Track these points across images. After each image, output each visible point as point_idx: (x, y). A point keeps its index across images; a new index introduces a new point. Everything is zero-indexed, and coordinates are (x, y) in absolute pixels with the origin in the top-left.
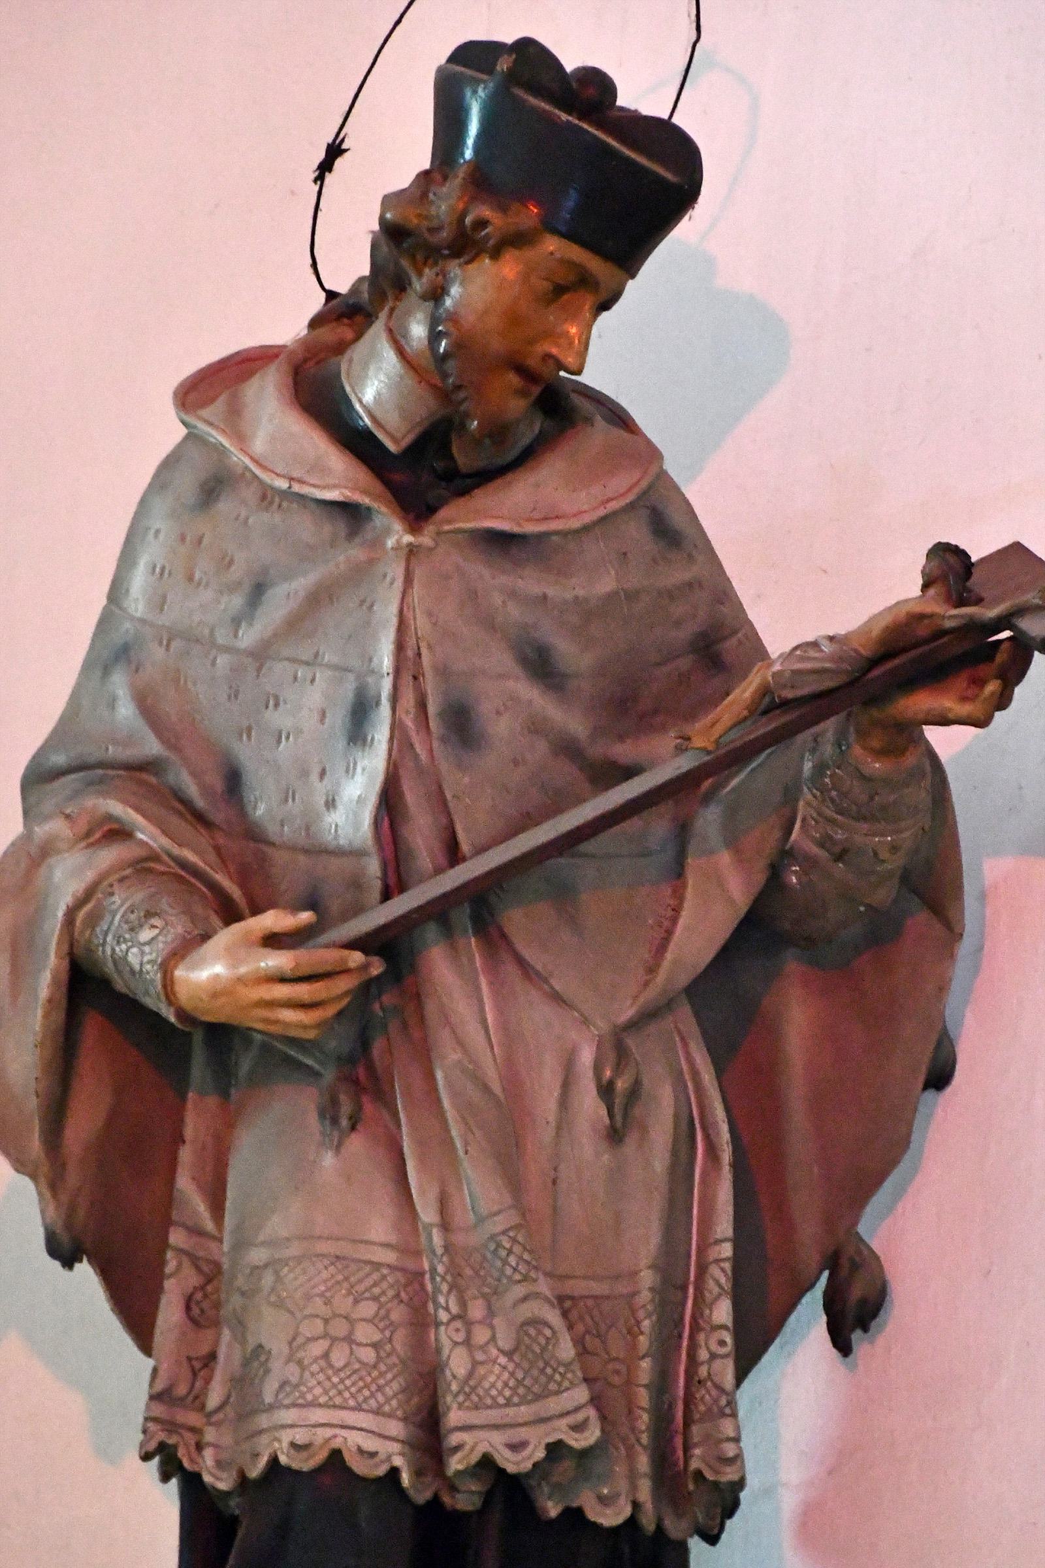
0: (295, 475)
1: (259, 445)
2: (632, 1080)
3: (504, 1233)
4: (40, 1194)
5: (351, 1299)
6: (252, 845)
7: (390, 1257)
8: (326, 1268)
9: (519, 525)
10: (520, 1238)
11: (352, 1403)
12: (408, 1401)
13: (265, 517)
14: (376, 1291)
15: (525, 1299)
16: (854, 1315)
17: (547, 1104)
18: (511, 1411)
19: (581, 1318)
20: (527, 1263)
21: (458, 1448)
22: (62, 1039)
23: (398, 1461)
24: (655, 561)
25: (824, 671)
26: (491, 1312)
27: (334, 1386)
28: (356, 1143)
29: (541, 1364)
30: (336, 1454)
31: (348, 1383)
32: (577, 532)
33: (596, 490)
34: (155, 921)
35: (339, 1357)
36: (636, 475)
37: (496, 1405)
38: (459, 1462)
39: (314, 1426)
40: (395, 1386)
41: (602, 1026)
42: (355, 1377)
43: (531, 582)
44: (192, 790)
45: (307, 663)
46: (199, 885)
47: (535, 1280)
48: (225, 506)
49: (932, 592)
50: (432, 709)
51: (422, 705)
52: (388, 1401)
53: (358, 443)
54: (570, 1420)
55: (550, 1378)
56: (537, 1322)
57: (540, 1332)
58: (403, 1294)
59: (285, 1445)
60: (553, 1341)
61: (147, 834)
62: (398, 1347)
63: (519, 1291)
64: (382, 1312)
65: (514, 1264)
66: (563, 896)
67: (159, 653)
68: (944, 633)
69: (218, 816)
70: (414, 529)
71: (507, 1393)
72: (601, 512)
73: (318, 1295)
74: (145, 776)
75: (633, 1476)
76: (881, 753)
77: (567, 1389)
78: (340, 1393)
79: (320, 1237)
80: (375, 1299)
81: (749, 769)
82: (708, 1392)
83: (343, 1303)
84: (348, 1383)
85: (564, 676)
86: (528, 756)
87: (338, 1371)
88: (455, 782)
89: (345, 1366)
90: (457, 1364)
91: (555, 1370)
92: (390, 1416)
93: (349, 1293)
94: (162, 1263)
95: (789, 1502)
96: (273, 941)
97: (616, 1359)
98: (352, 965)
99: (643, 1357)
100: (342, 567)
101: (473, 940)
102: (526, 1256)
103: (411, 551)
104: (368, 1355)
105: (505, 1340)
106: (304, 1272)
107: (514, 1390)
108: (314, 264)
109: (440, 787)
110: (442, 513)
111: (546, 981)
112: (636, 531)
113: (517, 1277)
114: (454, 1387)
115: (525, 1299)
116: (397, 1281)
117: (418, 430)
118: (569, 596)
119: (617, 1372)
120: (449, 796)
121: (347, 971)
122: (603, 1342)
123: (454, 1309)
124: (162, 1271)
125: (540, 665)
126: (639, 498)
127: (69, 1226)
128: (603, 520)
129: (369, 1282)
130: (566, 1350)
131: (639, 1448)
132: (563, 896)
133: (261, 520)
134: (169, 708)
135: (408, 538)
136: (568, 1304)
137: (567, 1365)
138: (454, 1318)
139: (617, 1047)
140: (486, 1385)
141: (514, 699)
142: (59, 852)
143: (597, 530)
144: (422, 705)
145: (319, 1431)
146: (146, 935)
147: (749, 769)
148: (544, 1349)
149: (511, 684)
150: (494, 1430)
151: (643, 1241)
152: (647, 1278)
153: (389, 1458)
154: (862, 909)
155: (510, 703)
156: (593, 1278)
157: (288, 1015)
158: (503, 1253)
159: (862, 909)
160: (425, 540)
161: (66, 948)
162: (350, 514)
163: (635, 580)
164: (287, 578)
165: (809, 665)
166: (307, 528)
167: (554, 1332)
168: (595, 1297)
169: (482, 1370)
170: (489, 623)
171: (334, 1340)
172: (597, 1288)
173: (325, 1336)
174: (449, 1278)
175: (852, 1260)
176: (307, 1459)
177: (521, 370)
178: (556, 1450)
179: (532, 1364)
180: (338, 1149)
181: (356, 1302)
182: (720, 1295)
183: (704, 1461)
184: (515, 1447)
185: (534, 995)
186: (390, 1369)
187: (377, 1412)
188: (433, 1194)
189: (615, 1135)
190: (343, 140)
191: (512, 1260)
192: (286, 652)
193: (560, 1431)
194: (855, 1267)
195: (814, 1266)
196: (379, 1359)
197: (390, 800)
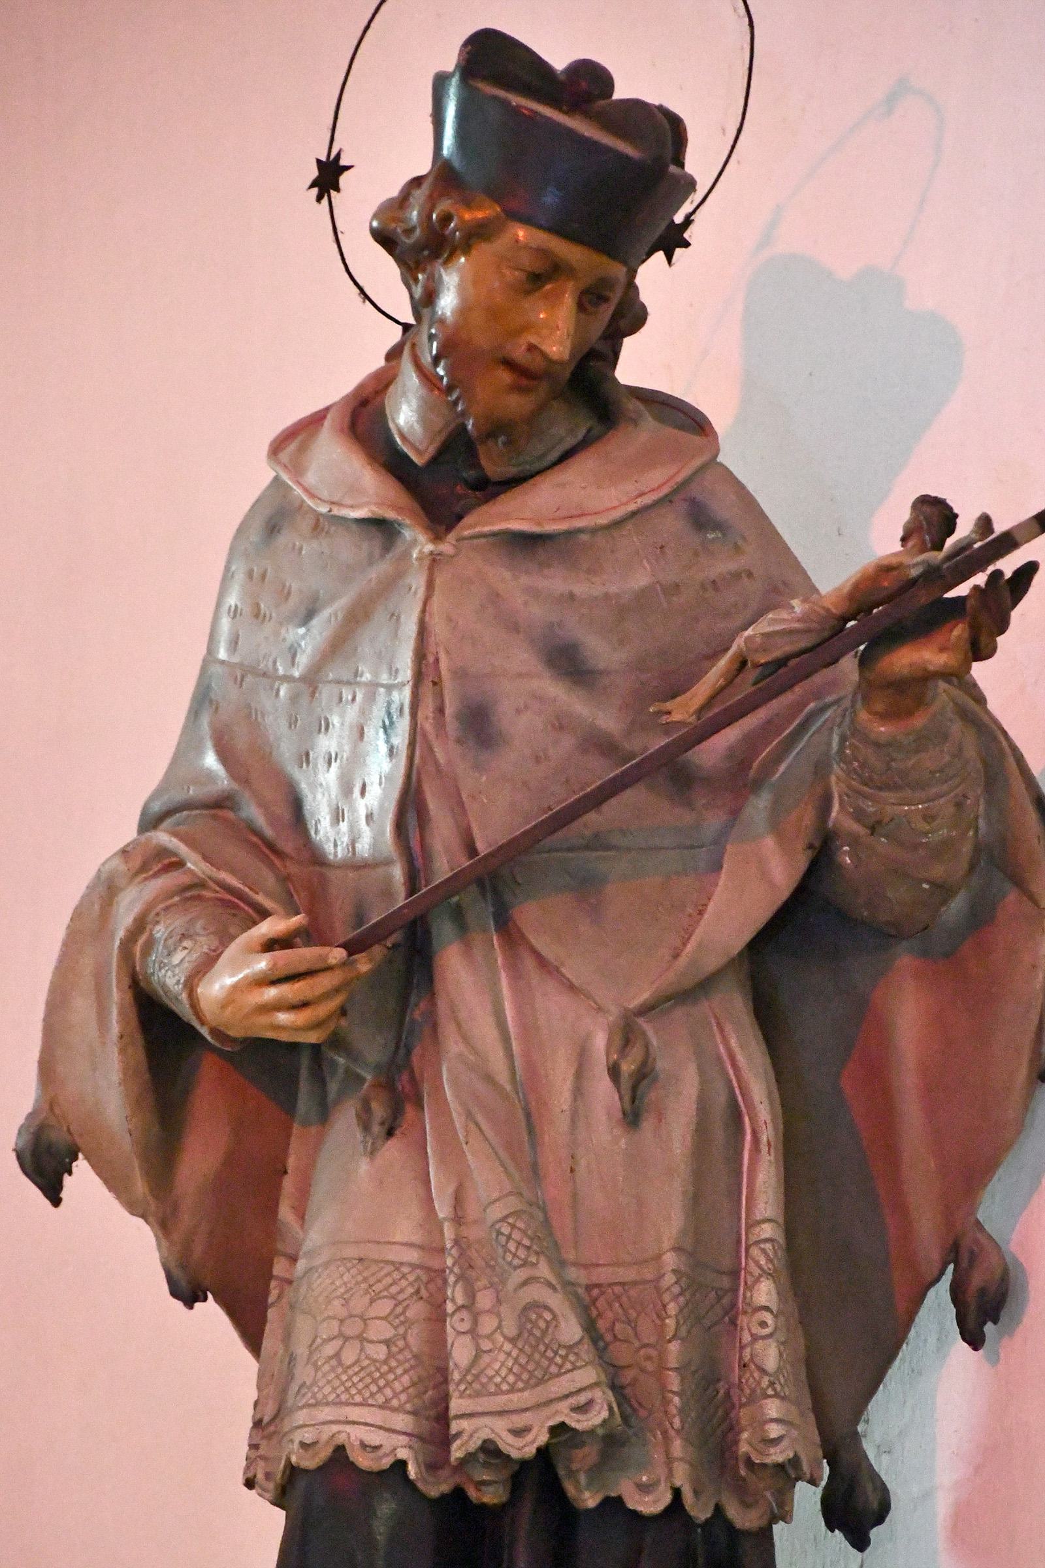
0: (336, 499)
1: (311, 478)
3: (504, 1219)
4: (156, 1236)
5: (367, 1298)
6: (317, 868)
7: (413, 1256)
8: (348, 1271)
9: (539, 524)
11: (358, 1399)
12: (420, 1395)
13: (315, 544)
15: (525, 1283)
16: (983, 1311)
18: (515, 1397)
19: (610, 1305)
20: (528, 1248)
21: (459, 1434)
23: (403, 1454)
24: (696, 554)
25: (791, 632)
27: (343, 1383)
28: (392, 1150)
29: (542, 1348)
30: (340, 1449)
31: (355, 1379)
33: (630, 488)
34: (186, 943)
35: (349, 1356)
36: (673, 469)
37: (499, 1392)
38: (459, 1448)
39: (324, 1423)
40: (406, 1380)
42: (362, 1374)
43: (557, 581)
44: (261, 821)
45: (349, 683)
46: (242, 905)
47: (534, 1265)
48: (284, 539)
49: (910, 544)
50: (449, 711)
51: (441, 710)
52: (396, 1395)
53: (391, 461)
54: (573, 1401)
56: (538, 1307)
57: (540, 1316)
58: (424, 1293)
59: (296, 1446)
60: (554, 1323)
61: (195, 864)
64: (399, 1309)
65: (513, 1249)
66: (586, 888)
68: (913, 582)
69: (288, 846)
70: (437, 538)
71: (511, 1379)
72: (632, 507)
73: (338, 1297)
74: (220, 812)
75: (669, 1461)
76: (884, 717)
77: (569, 1371)
78: (347, 1390)
79: (347, 1242)
81: (794, 753)
82: (752, 1375)
83: (359, 1303)
84: (355, 1379)
85: (591, 672)
86: (551, 752)
88: (469, 780)
89: (354, 1365)
90: (461, 1353)
91: (556, 1353)
92: (394, 1410)
93: (367, 1292)
94: (267, 1293)
95: (943, 1506)
96: (270, 945)
98: (332, 961)
99: (669, 1341)
100: (373, 583)
101: (495, 938)
102: (526, 1242)
103: (434, 560)
104: (380, 1352)
105: (511, 1329)
106: (329, 1276)
107: (518, 1377)
108: (366, 297)
109: (458, 789)
110: (467, 520)
111: (557, 969)
112: (672, 523)
113: (516, 1262)
114: (456, 1376)
115: (525, 1283)
116: (418, 1278)
117: (439, 440)
118: (597, 591)
119: (649, 1358)
120: (464, 797)
121: (329, 968)
122: (634, 1329)
123: (460, 1300)
124: (266, 1300)
125: (566, 661)
126: (675, 492)
127: (183, 1266)
128: (634, 514)
129: (389, 1280)
130: (571, 1330)
131: (672, 1433)
133: (310, 548)
134: (241, 742)
135: (429, 547)
136: (595, 1292)
138: (459, 1309)
139: (627, 1033)
141: (540, 698)
142: (122, 889)
143: (629, 526)
145: (325, 1428)
146: (177, 958)
147: (794, 753)
148: (544, 1332)
149: (535, 684)
150: (502, 1419)
151: (669, 1222)
154: (925, 886)
156: (617, 1264)
157: (283, 1017)
158: (503, 1239)
159: (925, 886)
160: (446, 547)
161: (127, 981)
162: (381, 529)
163: (670, 575)
164: (333, 598)
165: (778, 628)
166: (348, 548)
167: (555, 1317)
168: (622, 1284)
169: (486, 1358)
171: (347, 1339)
173: (341, 1334)
174: (456, 1270)
175: (972, 1252)
176: (314, 1456)
179: (535, 1348)
180: (372, 1153)
182: (760, 1276)
183: (750, 1444)
184: (518, 1433)
185: (551, 986)
186: (400, 1363)
189: (632, 1117)
190: (338, 156)
191: (512, 1246)
193: (563, 1414)
196: (390, 1355)
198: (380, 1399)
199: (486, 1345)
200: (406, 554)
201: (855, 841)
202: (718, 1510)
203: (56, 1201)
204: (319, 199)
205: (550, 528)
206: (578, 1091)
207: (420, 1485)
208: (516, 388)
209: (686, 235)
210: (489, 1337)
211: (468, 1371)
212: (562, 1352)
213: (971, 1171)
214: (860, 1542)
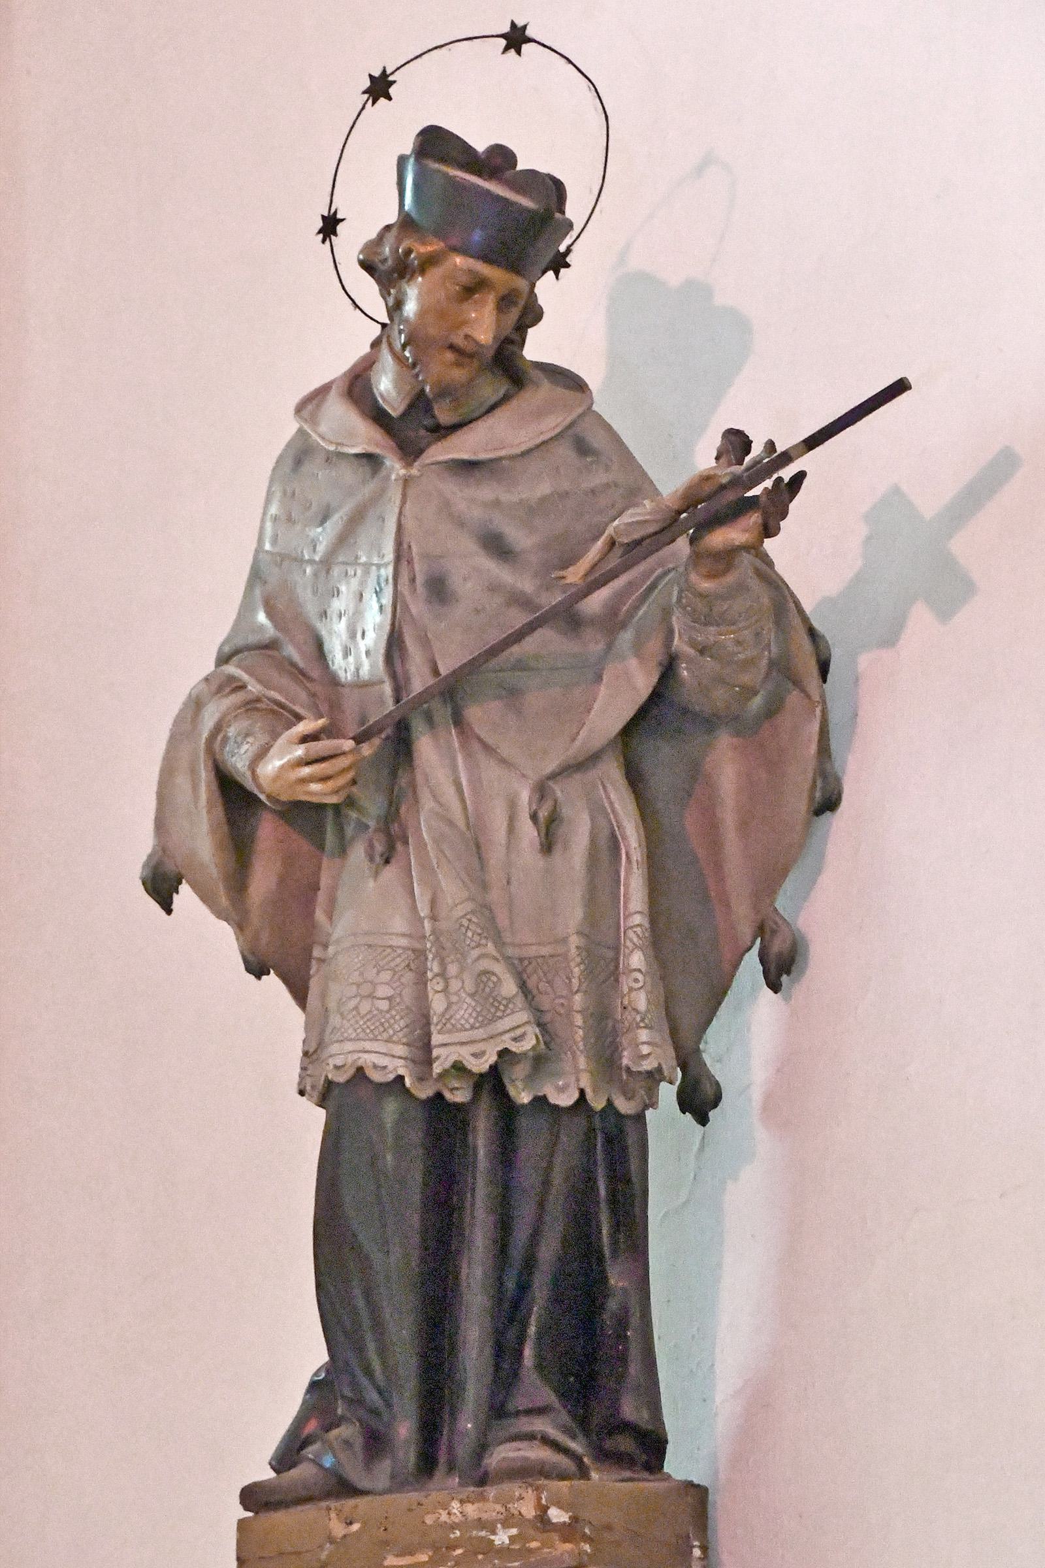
1: (323, 428)
2: (550, 809)
3: (463, 917)
7: (404, 942)
10: (474, 919)
11: (371, 1036)
12: (412, 1032)
14: (392, 964)
16: (780, 970)
17: (499, 832)
21: (437, 1058)
22: (226, 828)
23: (401, 1071)
25: (645, 521)
26: (462, 969)
30: (360, 1070)
32: (517, 456)
34: (250, 739)
40: (402, 1023)
41: (534, 777)
44: (297, 658)
48: (306, 468)
53: (379, 417)
54: (512, 1034)
55: (497, 1009)
57: (489, 979)
61: (254, 688)
62: (406, 999)
63: (475, 953)
67: (276, 570)
68: (723, 487)
70: (409, 465)
76: (710, 576)
80: (392, 969)
83: (371, 973)
87: (362, 1018)
90: (438, 1004)
94: (308, 967)
95: (757, 1095)
97: (562, 997)
104: (384, 1005)
105: (470, 986)
112: (565, 452)
113: (473, 944)
115: (479, 958)
118: (515, 498)
121: (344, 753)
125: (496, 546)
128: (538, 446)
132: (512, 694)
134: (280, 605)
135: (403, 472)
137: (510, 1000)
139: (541, 791)
140: (458, 1017)
144: (413, 580)
146: (245, 747)
148: (492, 992)
150: (465, 1046)
152: (574, 941)
153: (395, 1069)
155: (472, 570)
157: (315, 787)
161: (210, 763)
162: (371, 460)
163: (566, 485)
166: (349, 474)
167: (499, 979)
169: (454, 1007)
170: (460, 523)
172: (545, 951)
177: (452, 347)
178: (504, 1053)
181: (378, 972)
187: (388, 1041)
188: (428, 897)
189: (548, 846)
190: (336, 212)
191: (470, 934)
192: (341, 559)
194: (774, 932)
195: (748, 939)
197: (394, 645)
198: (385, 1036)
199: (454, 999)
200: (388, 477)
201: (690, 661)
202: (610, 1103)
203: (169, 911)
204: (324, 241)
205: (482, 456)
206: (511, 829)
207: (413, 1091)
208: (458, 364)
209: (568, 259)
210: (456, 994)
211: (443, 1015)
212: (504, 1002)
213: (771, 877)
214: (703, 1120)
